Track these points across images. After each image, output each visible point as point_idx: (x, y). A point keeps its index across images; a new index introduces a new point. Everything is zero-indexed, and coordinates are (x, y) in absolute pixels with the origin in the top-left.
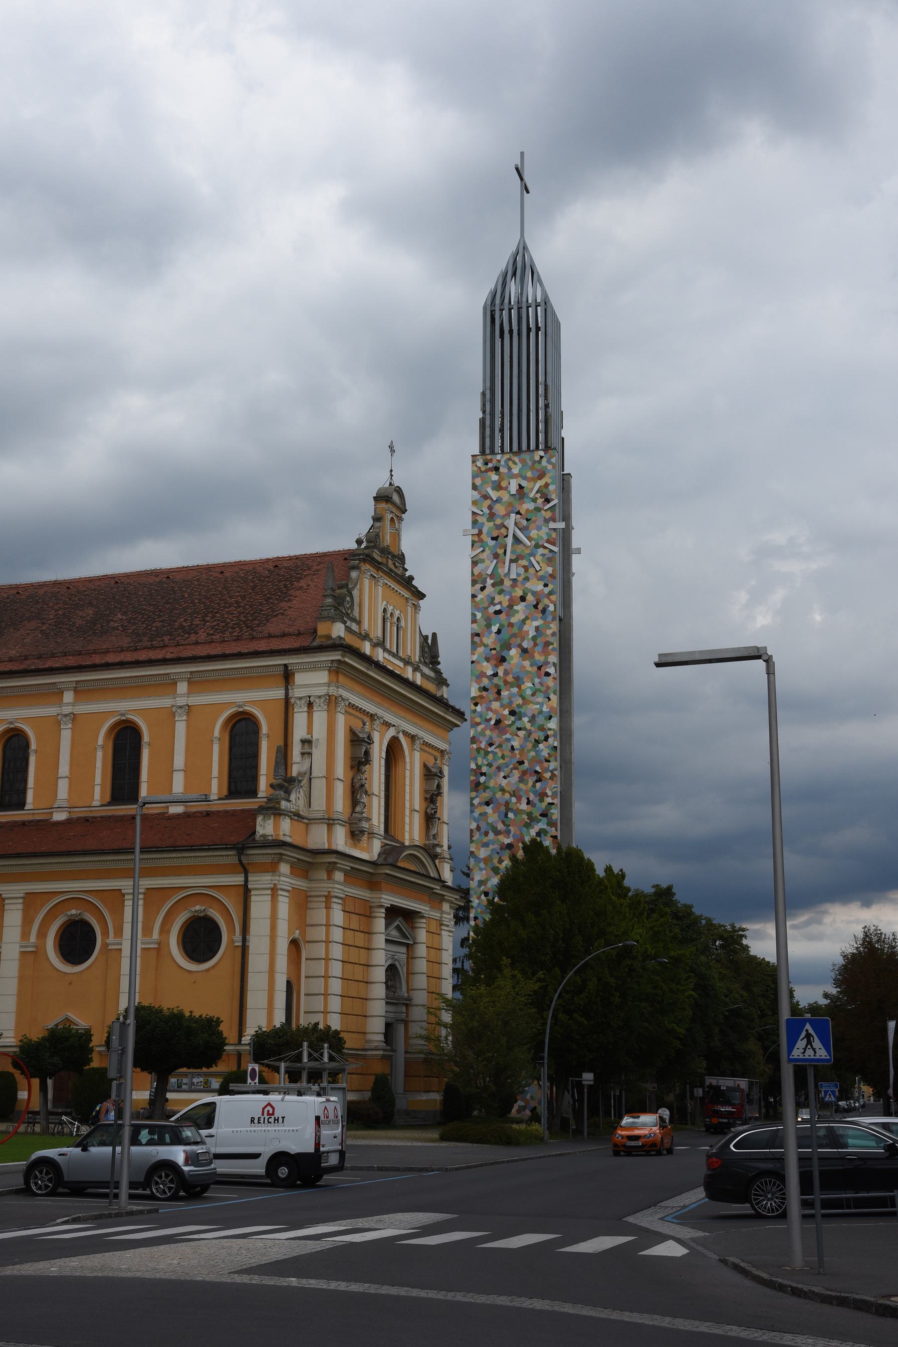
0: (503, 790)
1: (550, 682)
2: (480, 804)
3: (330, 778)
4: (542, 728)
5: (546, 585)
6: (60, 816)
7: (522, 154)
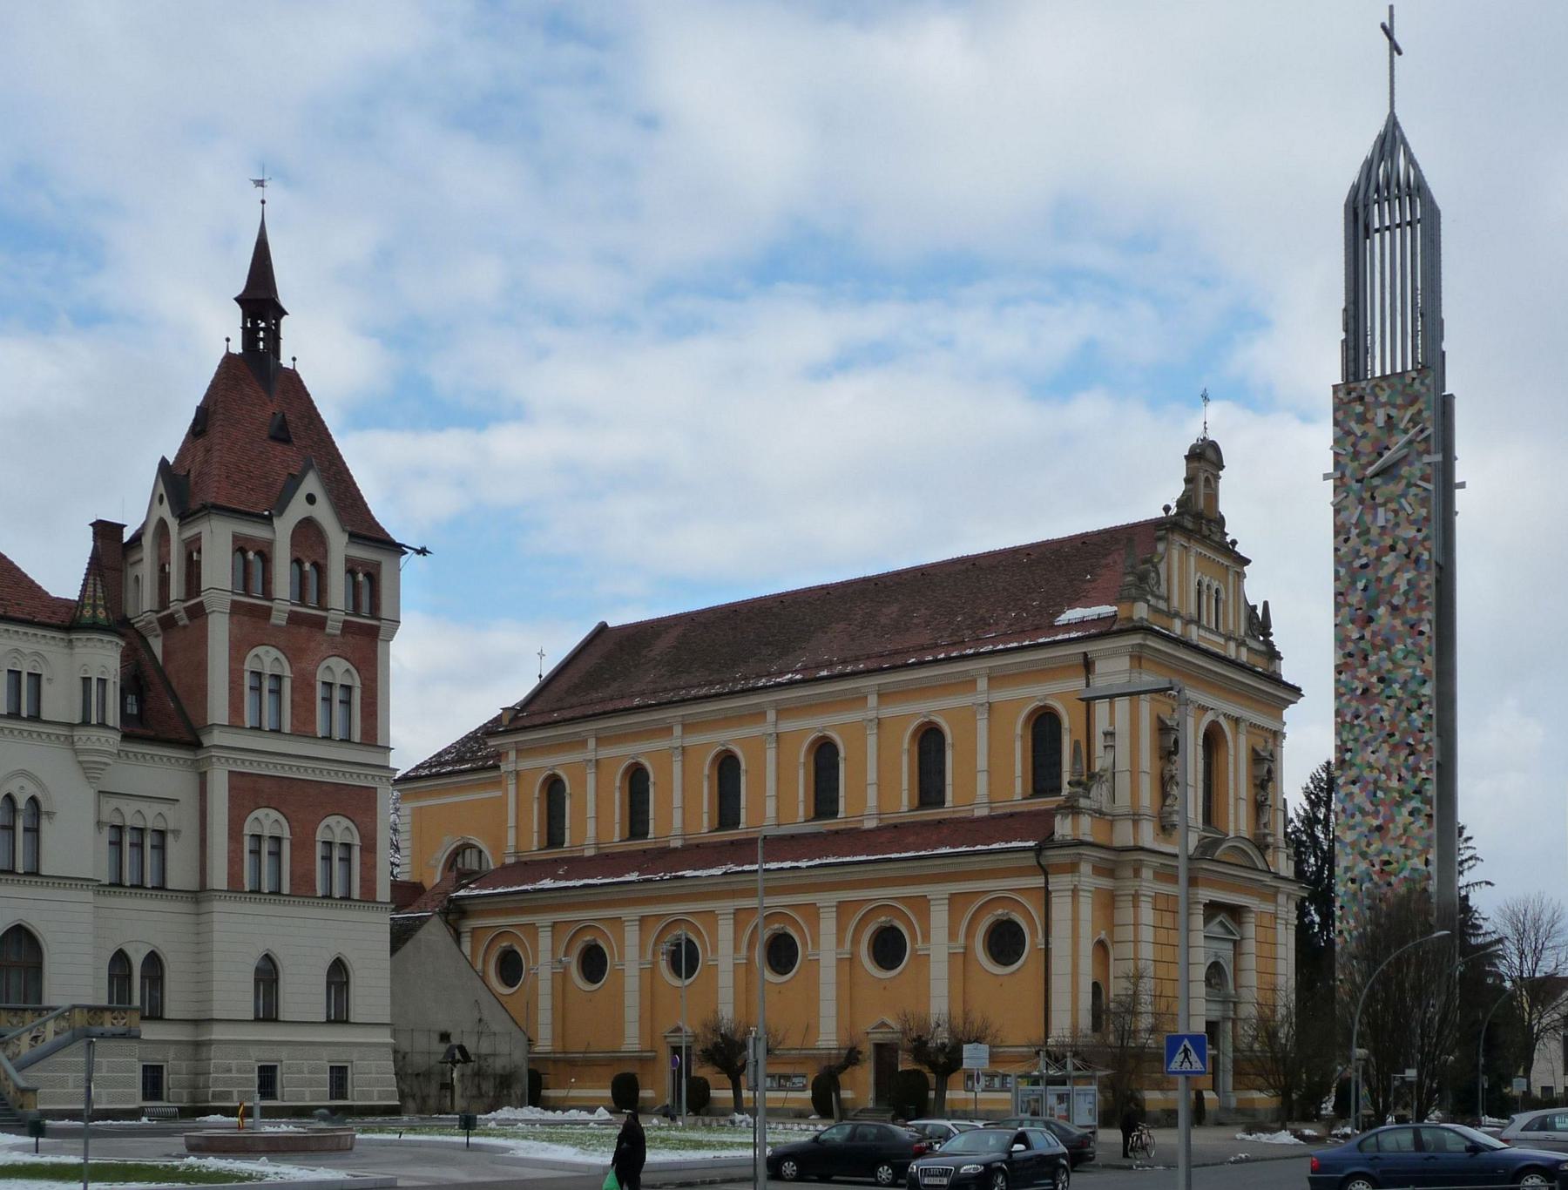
0: (1370, 766)
1: (1423, 641)
2: (1346, 784)
3: (1134, 772)
4: (1415, 695)
5: (1419, 530)
6: (870, 824)
7: (1391, 8)
